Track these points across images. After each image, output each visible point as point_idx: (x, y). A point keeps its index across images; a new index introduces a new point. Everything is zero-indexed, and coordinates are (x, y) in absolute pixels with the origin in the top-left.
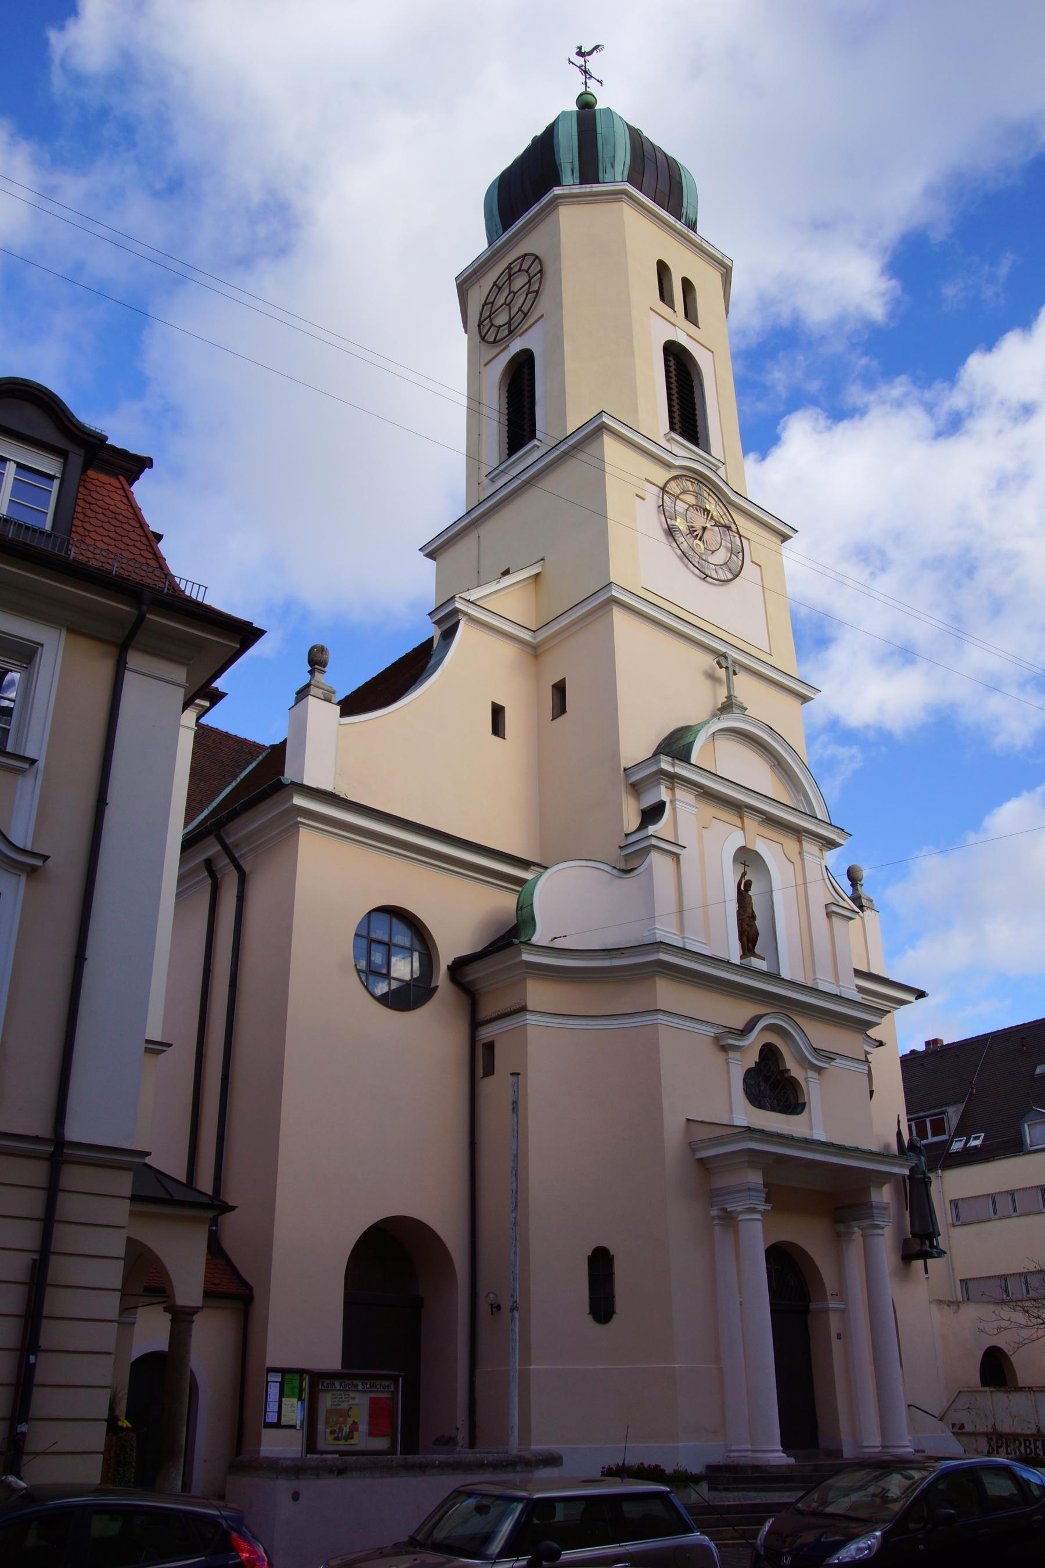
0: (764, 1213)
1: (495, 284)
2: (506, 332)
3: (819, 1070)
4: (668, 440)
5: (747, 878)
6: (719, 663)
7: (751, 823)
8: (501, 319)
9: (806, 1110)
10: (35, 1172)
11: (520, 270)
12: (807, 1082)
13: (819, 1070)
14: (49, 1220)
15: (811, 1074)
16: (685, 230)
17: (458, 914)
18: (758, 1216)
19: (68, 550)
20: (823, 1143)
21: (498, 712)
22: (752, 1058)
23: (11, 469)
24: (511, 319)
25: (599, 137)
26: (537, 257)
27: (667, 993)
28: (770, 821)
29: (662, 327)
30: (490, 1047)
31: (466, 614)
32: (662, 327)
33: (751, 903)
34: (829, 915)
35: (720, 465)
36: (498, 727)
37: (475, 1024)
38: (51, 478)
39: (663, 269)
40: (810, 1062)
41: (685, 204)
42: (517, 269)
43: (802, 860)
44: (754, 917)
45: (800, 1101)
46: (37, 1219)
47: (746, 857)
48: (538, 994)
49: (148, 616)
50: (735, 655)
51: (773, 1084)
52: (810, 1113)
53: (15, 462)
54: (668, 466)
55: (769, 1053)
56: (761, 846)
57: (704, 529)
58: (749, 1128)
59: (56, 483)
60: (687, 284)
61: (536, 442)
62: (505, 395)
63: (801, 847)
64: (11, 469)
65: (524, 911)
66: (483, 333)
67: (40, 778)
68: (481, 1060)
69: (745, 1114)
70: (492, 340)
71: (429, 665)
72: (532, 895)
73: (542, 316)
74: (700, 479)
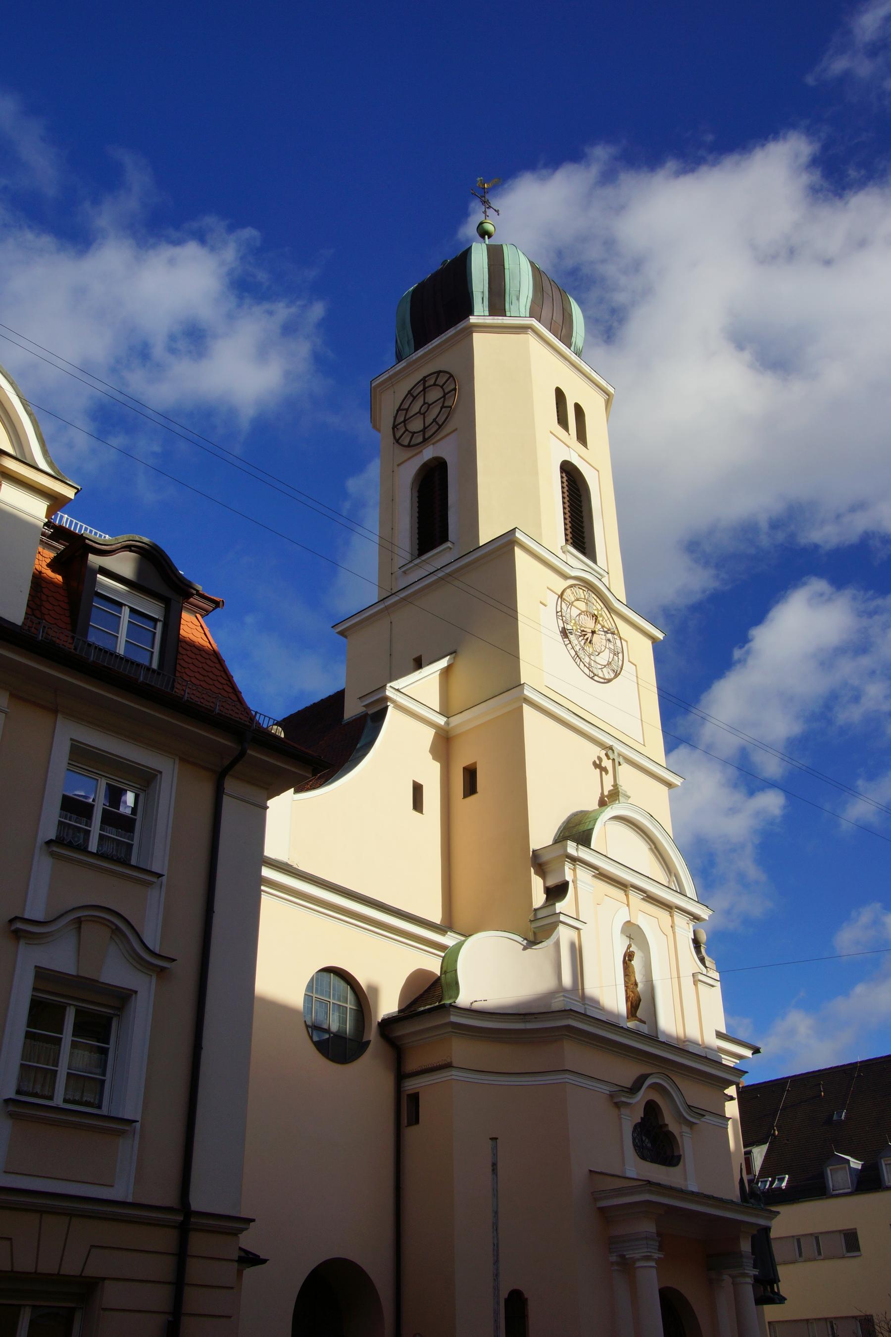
0: (658, 1261)
1: (409, 392)
2: (420, 439)
3: (691, 1125)
4: (564, 552)
5: (631, 949)
6: (607, 755)
7: (635, 898)
8: (416, 425)
9: (681, 1163)
10: (165, 1240)
11: (435, 384)
12: (682, 1136)
13: (691, 1125)
14: (179, 1284)
15: (685, 1129)
16: (574, 357)
17: (387, 973)
18: (653, 1264)
19: (173, 687)
20: (693, 1193)
21: (418, 789)
22: (639, 1114)
23: (126, 611)
24: (425, 428)
25: (507, 272)
26: (451, 376)
27: (574, 1055)
28: (650, 898)
29: (559, 447)
30: (415, 1098)
31: (394, 702)
32: (559, 447)
33: (634, 972)
34: (695, 982)
35: (605, 574)
36: (418, 805)
37: (401, 1076)
38: (155, 620)
39: (560, 396)
40: (684, 1118)
41: (574, 334)
42: (432, 382)
43: (674, 933)
44: (636, 984)
45: (676, 1154)
46: (169, 1283)
47: (632, 931)
48: (460, 1050)
49: (249, 752)
50: (619, 748)
51: (656, 1140)
52: (684, 1166)
53: (129, 607)
54: (565, 577)
55: (651, 1108)
56: (642, 921)
57: (593, 632)
58: (649, 1182)
59: (159, 625)
60: (578, 409)
61: (449, 544)
62: (416, 494)
63: (673, 921)
64: (126, 611)
65: (448, 975)
66: (398, 436)
67: (164, 889)
68: (407, 1109)
69: (636, 1168)
70: (406, 443)
71: (359, 746)
72: (456, 961)
73: (456, 430)
74: (589, 586)
